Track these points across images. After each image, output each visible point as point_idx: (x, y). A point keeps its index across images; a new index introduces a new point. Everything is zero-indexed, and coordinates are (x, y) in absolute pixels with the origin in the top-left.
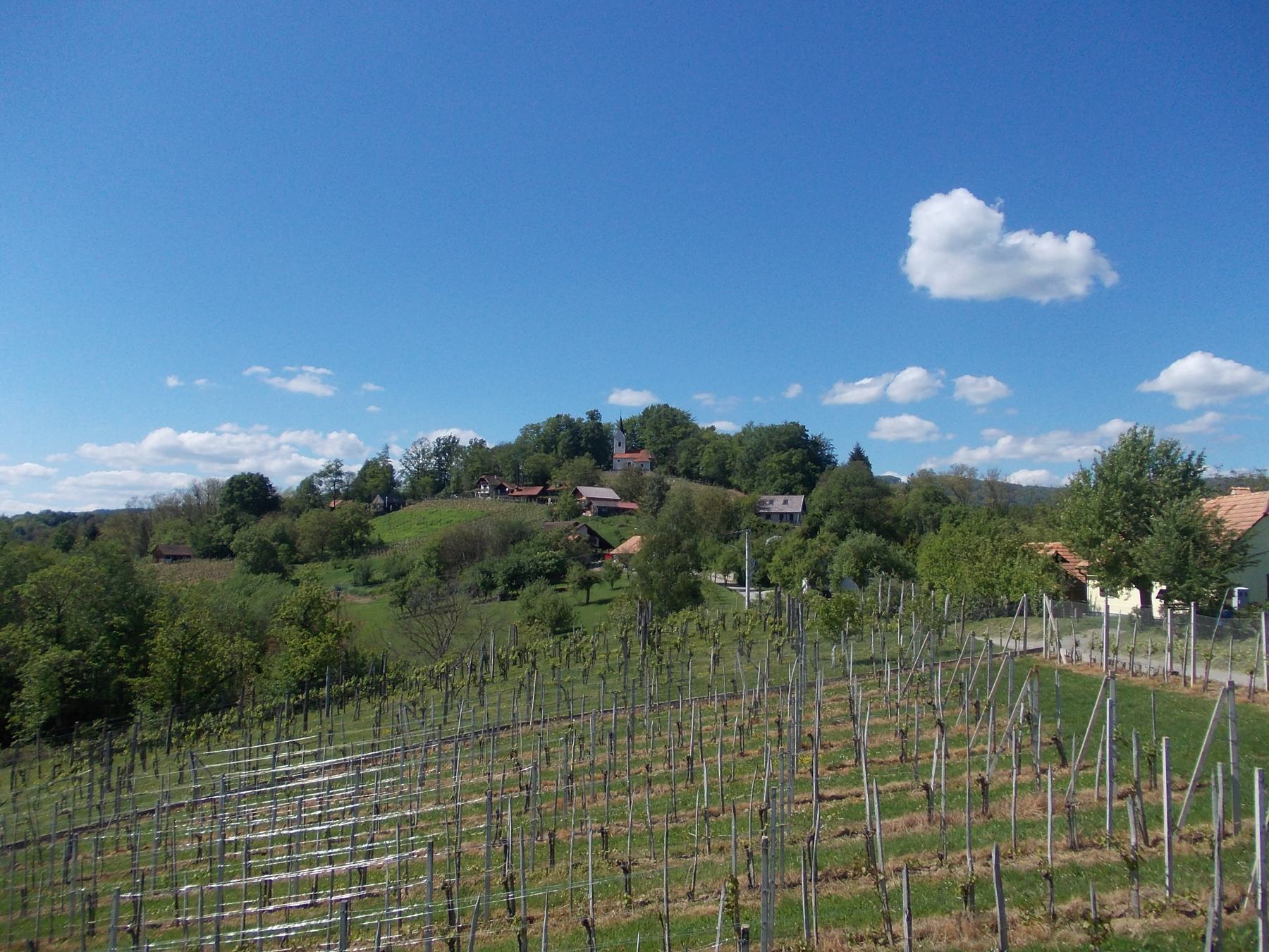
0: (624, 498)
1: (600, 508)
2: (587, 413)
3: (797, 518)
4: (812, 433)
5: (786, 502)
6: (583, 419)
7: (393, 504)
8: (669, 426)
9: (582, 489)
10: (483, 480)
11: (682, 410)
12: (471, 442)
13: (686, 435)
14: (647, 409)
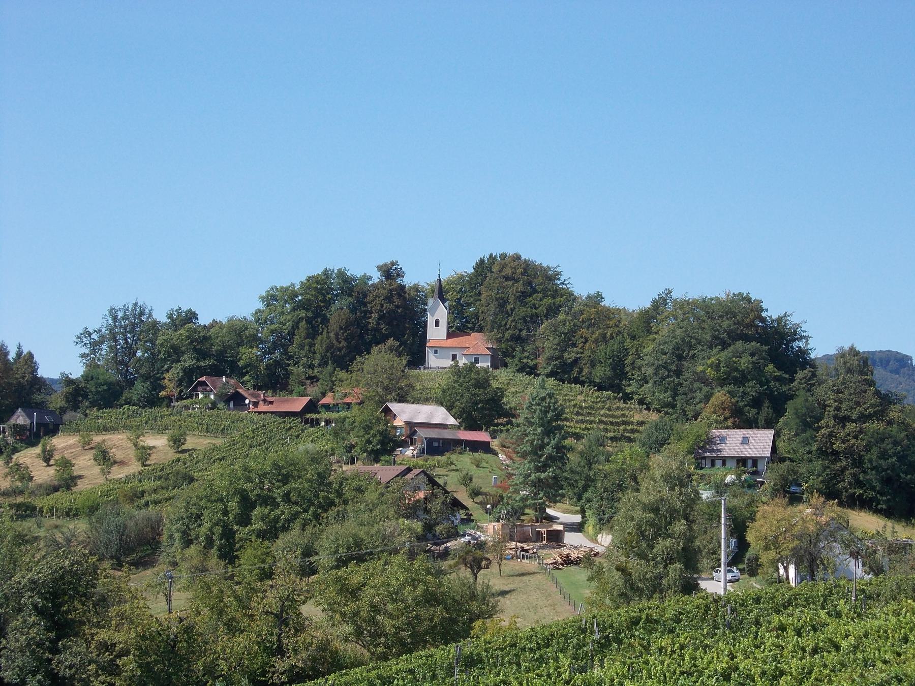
0: (471, 425)
1: (430, 441)
2: (379, 268)
3: (762, 466)
4: (772, 311)
5: (745, 441)
6: (370, 278)
7: (46, 425)
8: (523, 297)
9: (395, 407)
10: (203, 384)
11: (545, 265)
12: (170, 316)
13: (553, 311)
14: (482, 261)
